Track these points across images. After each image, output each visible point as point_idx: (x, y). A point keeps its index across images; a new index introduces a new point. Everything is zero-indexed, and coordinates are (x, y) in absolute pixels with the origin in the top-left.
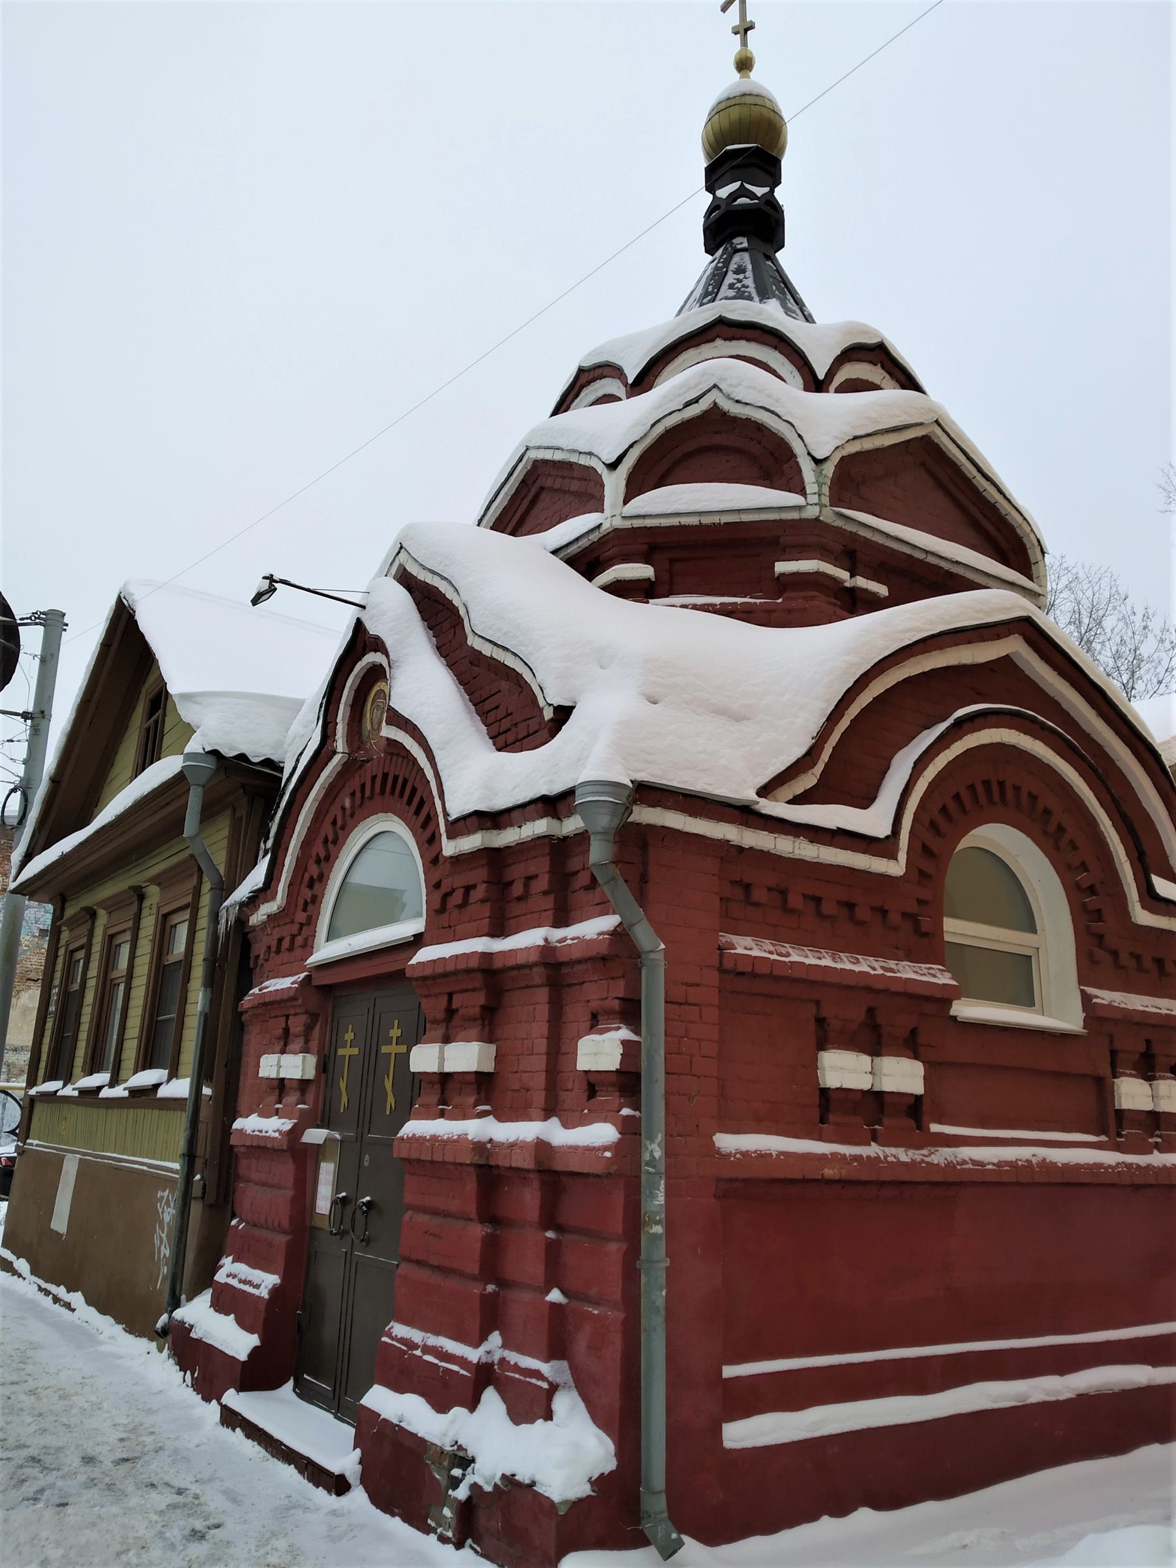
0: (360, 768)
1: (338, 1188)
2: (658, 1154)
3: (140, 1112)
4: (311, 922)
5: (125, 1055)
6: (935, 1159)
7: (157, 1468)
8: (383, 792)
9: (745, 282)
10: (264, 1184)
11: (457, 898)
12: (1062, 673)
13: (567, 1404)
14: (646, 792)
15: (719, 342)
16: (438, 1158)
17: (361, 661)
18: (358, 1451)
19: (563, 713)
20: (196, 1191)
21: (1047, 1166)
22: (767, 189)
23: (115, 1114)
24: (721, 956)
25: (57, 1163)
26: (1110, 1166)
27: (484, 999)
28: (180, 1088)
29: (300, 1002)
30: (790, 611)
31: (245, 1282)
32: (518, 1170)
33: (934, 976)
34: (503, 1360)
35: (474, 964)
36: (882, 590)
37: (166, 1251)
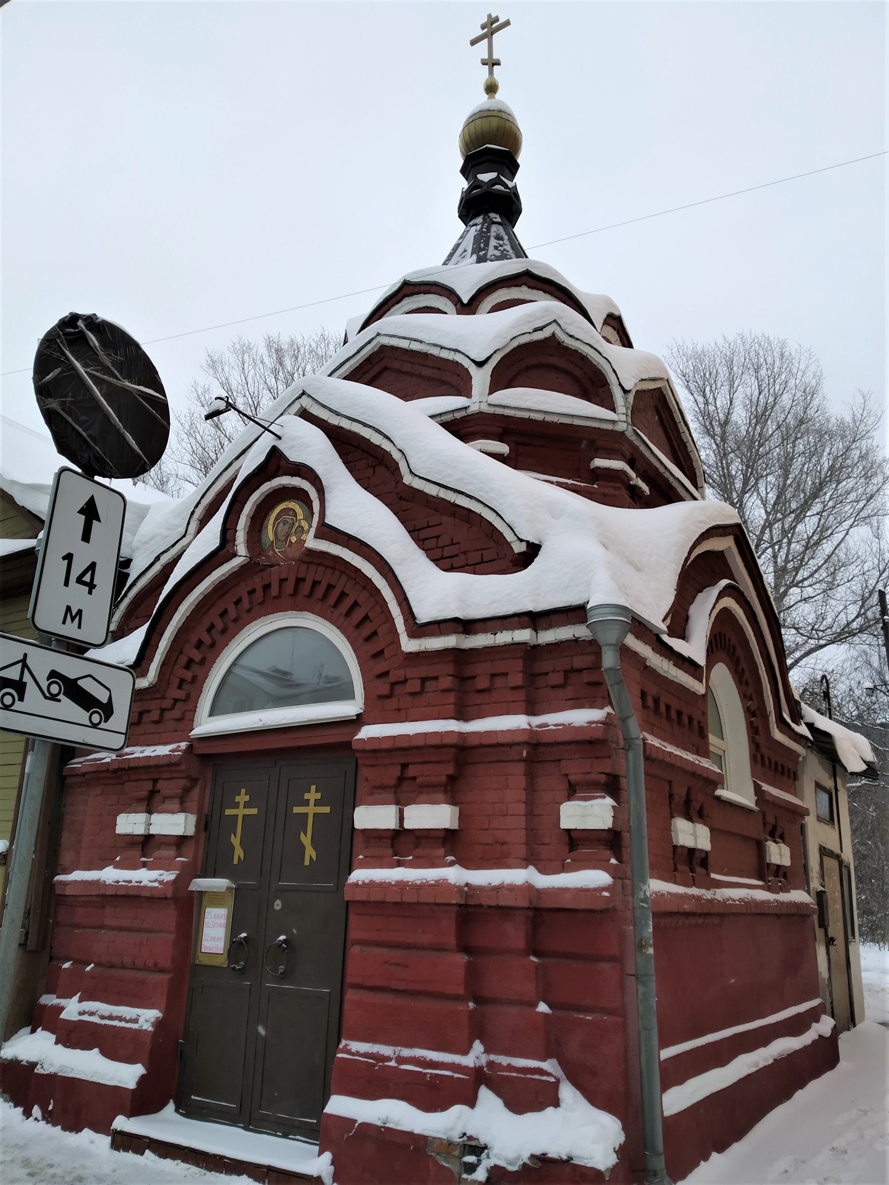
0: (262, 570)
9: (505, 247)
15: (524, 288)
19: (533, 550)
27: (454, 768)
29: (183, 767)
34: (491, 1064)
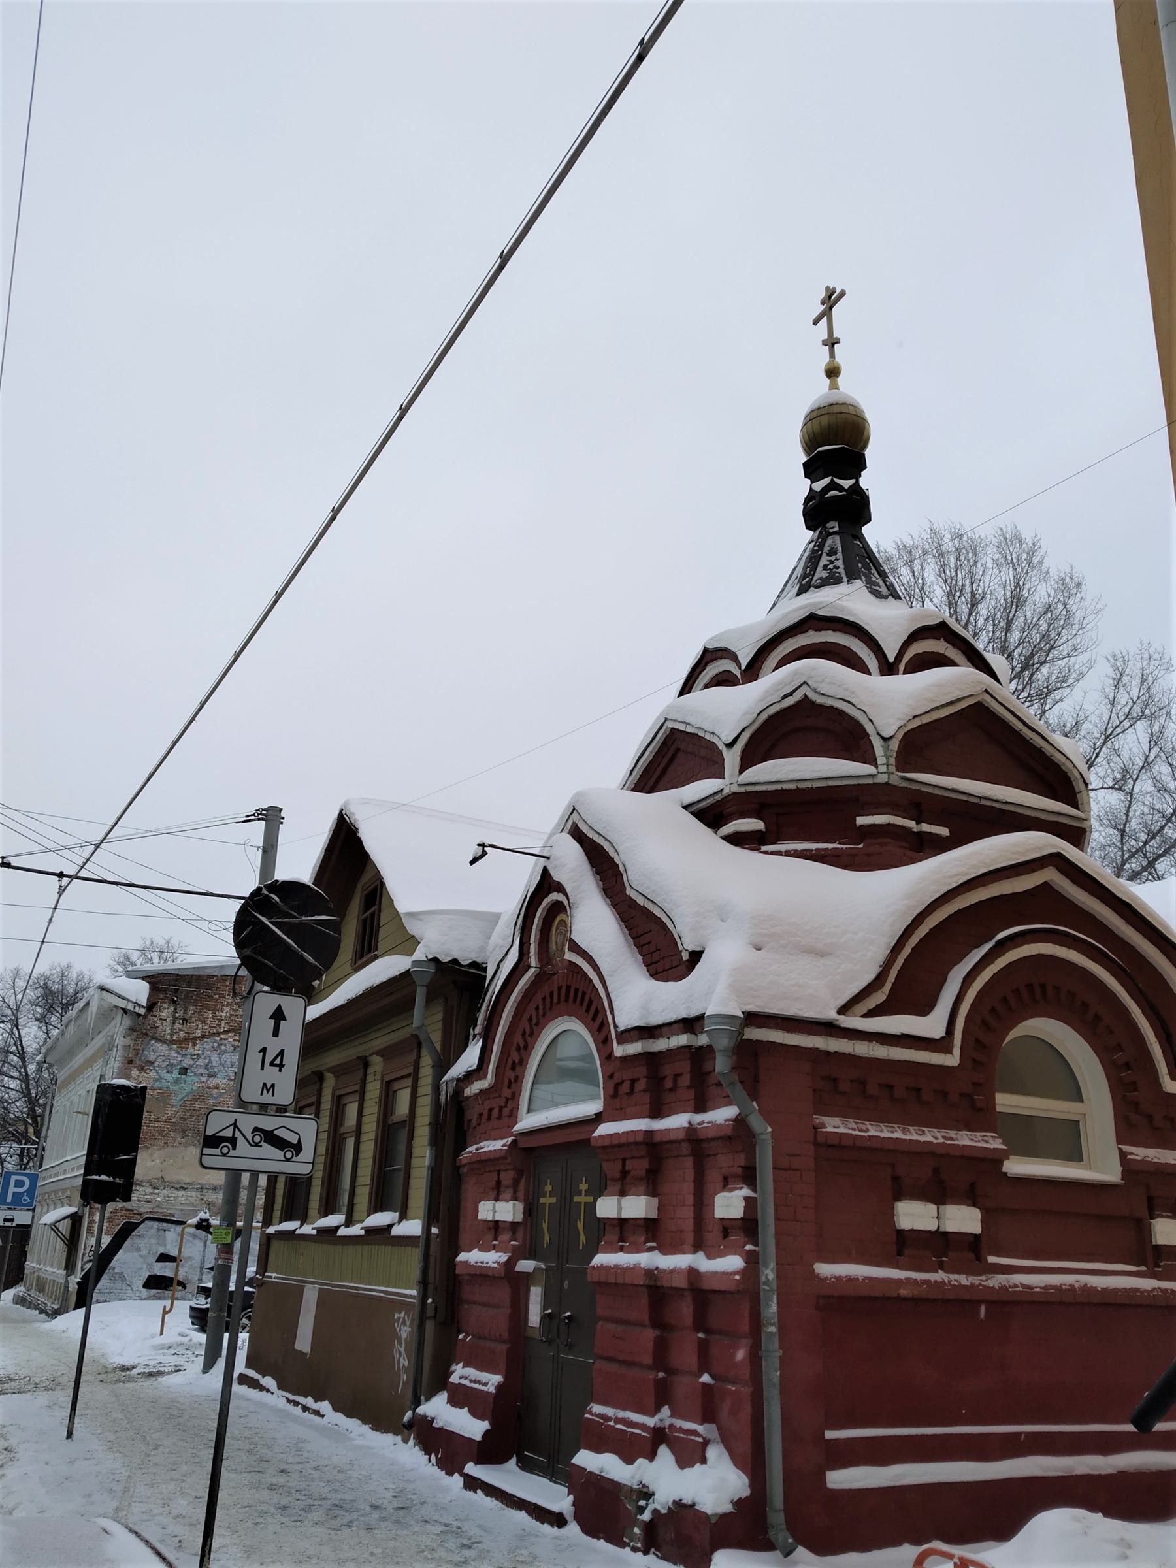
1: (545, 1307)
2: (771, 1276)
3: (375, 1248)
4: (515, 1097)
5: (357, 1199)
6: (991, 1283)
7: (425, 1512)
8: (567, 1000)
10: (484, 1305)
11: (625, 1088)
12: (1092, 893)
13: (715, 1453)
14: (753, 1018)
16: (620, 1281)
17: (545, 904)
18: (571, 1497)
19: (696, 956)
20: (430, 1312)
21: (1087, 1290)
22: (853, 481)
23: (350, 1250)
24: (816, 1133)
25: (295, 1294)
26: (1146, 1291)
27: (647, 1163)
28: (412, 1227)
29: (509, 1161)
30: (869, 855)
31: (475, 1382)
32: (676, 1289)
33: (987, 1142)
34: (671, 1425)
35: (640, 1138)
36: (944, 831)
37: (404, 1362)
